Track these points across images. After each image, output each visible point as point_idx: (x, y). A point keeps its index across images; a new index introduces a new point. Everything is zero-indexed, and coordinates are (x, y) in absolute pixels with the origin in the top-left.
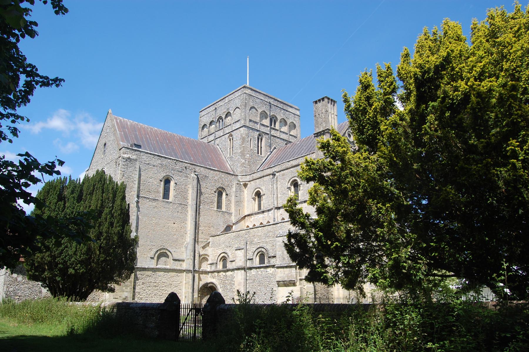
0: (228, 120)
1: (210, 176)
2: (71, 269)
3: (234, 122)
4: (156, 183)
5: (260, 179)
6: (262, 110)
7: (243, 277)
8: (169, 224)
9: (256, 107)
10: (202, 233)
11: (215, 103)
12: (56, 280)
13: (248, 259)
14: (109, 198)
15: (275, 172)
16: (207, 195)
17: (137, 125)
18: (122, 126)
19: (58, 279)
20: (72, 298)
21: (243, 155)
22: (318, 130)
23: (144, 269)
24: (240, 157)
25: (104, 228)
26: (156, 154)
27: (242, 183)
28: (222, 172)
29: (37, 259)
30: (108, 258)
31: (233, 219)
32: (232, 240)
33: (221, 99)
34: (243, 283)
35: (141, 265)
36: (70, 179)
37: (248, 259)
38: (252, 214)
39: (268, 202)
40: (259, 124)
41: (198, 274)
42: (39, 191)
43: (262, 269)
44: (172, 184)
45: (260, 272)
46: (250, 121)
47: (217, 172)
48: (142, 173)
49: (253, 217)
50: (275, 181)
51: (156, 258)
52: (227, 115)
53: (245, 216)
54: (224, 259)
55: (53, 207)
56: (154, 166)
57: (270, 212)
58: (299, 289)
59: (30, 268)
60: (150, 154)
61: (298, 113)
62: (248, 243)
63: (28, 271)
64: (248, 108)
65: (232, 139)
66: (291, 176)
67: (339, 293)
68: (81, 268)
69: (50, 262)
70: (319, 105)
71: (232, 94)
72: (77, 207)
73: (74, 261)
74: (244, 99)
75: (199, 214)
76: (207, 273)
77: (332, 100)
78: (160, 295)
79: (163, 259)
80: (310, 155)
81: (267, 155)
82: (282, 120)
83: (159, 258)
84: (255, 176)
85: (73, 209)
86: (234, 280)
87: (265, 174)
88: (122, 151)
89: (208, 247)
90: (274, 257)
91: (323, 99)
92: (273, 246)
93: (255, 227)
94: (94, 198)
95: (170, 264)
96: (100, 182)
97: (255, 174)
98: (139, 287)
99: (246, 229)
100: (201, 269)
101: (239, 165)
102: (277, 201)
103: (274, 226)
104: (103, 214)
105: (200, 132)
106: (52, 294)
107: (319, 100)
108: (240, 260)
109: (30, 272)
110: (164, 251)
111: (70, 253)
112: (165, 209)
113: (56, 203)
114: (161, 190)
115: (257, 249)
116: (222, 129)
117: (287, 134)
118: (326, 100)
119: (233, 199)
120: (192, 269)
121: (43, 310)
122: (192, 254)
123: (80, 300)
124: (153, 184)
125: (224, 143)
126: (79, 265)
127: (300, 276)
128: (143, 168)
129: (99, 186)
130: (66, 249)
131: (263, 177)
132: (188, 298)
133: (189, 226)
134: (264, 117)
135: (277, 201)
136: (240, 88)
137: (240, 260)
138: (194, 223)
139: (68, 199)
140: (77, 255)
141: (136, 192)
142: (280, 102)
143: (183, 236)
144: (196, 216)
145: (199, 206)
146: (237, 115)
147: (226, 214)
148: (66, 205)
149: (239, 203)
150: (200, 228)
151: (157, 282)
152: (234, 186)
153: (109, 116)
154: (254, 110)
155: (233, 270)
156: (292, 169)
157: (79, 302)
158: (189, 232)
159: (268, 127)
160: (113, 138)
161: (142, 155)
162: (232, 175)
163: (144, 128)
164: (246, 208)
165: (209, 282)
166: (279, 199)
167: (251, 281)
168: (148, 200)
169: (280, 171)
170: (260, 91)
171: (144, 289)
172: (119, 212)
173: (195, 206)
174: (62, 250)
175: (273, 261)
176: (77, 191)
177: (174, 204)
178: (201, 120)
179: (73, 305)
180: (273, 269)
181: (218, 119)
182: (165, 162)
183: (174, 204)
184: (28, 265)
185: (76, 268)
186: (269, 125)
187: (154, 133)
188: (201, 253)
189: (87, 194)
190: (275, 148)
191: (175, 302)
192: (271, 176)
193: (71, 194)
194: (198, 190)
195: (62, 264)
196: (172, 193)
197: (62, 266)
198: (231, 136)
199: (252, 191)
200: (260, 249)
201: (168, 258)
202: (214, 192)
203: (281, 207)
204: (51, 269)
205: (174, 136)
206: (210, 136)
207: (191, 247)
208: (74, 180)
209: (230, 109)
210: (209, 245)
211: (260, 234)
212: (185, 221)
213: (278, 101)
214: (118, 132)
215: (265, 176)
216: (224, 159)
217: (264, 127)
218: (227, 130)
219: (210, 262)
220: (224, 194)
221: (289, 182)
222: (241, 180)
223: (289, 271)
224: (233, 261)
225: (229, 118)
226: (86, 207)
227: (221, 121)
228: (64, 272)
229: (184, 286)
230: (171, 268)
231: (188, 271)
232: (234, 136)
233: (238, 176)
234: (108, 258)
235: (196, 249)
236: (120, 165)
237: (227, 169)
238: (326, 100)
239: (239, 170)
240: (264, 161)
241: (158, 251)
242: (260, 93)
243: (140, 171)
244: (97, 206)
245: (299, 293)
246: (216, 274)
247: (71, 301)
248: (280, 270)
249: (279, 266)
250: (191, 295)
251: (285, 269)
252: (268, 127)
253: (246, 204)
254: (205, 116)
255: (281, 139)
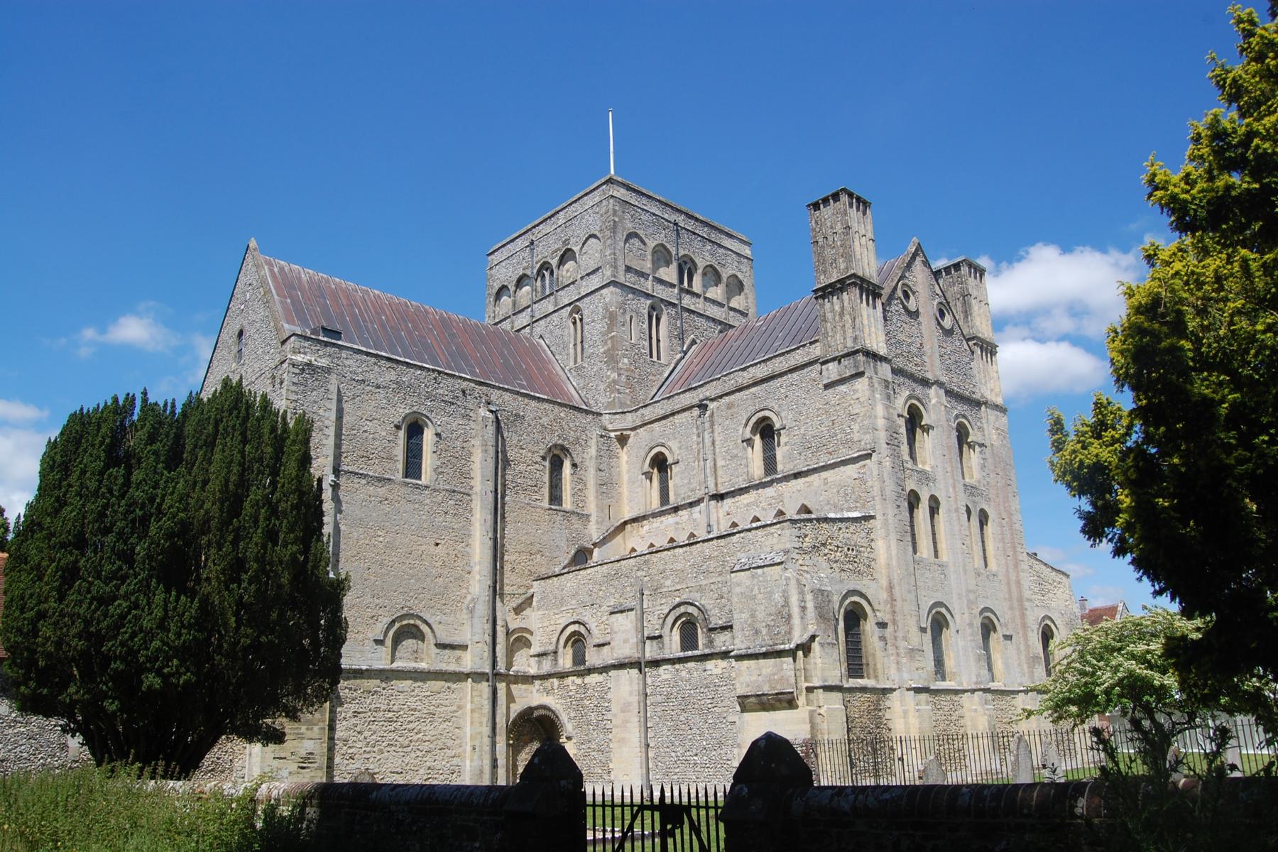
0: (568, 271)
1: (530, 416)
2: (151, 676)
3: (584, 274)
4: (384, 434)
5: (664, 422)
6: (656, 243)
7: (636, 687)
8: (423, 548)
9: (641, 233)
10: (513, 570)
11: (530, 230)
12: (103, 709)
13: (649, 638)
14: (262, 458)
15: (707, 399)
16: (522, 467)
17: (327, 282)
18: (287, 285)
19: (111, 706)
20: (155, 769)
21: (611, 358)
22: (823, 281)
23: (358, 674)
24: (604, 367)
25: (251, 548)
26: (384, 354)
27: (612, 435)
28: (560, 404)
29: (44, 645)
30: (263, 639)
31: (594, 532)
32: (598, 587)
33: (546, 216)
34: (636, 705)
35: (350, 662)
36: (145, 400)
37: (649, 638)
38: (644, 517)
39: (689, 483)
40: (651, 278)
41: (504, 684)
42: (50, 439)
43: (691, 665)
44: (428, 436)
45: (684, 674)
46: (628, 269)
47: (546, 406)
48: (345, 406)
49: (647, 526)
50: (707, 425)
51: (389, 642)
52: (562, 256)
53: (625, 523)
54: (577, 641)
55: (93, 485)
56: (378, 387)
57: (697, 509)
58: (806, 715)
59: (24, 675)
60: (368, 354)
61: (747, 251)
62: (646, 592)
63: (17, 684)
64: (621, 236)
65: (581, 320)
66: (752, 409)
67: (906, 723)
68: (183, 670)
69: (83, 654)
70: (826, 212)
71: (575, 201)
72: (166, 482)
73: (158, 650)
74: (611, 212)
75: (503, 517)
76: (528, 679)
77: (859, 200)
78: (402, 746)
79: (409, 644)
80: (806, 349)
81: (674, 361)
82: (709, 269)
83: (397, 641)
84: (649, 413)
85: (154, 488)
86: (609, 696)
87: (677, 407)
88: (288, 346)
89: (529, 609)
90: (727, 628)
91: (836, 197)
92: (722, 597)
93: (673, 545)
94: (217, 456)
95: (430, 659)
96: (235, 412)
97: (649, 408)
98: (344, 723)
99: (668, 546)
100: (513, 669)
101: (602, 387)
102: (716, 479)
103: (722, 542)
104: (247, 505)
105: (491, 307)
106: (93, 754)
107: (825, 201)
108: (626, 641)
109: (23, 688)
110: (412, 622)
111: (146, 623)
112: (410, 507)
113: (102, 473)
114: (399, 452)
115: (674, 608)
116: (552, 294)
117: (721, 305)
118: (844, 198)
119: (591, 476)
120: (487, 670)
121: (60, 809)
122: (488, 627)
123: (180, 773)
124: (377, 436)
125: (557, 332)
126: (175, 662)
127: (806, 680)
128: (348, 394)
129: (231, 424)
130: (134, 612)
131: (673, 414)
132: (481, 751)
133: (478, 551)
134: (662, 263)
135: (716, 479)
136: (596, 185)
137: (626, 641)
138: (490, 543)
139: (139, 462)
140: (169, 631)
141: (331, 458)
142: (702, 222)
143: (461, 578)
144: (496, 522)
145: (503, 497)
146: (591, 255)
147: (574, 519)
148: (133, 478)
149: (607, 486)
150: (506, 558)
151: (395, 708)
152: (593, 443)
153: (249, 258)
154: (635, 241)
155: (604, 669)
156: (753, 390)
157: (179, 779)
158: (477, 568)
159: (672, 286)
160: (262, 312)
161: (344, 355)
162: (587, 412)
163: (346, 291)
164: (626, 501)
165: (534, 703)
166: (720, 472)
167: (659, 698)
168: (364, 482)
169: (721, 397)
170: (651, 194)
171: (358, 729)
172: (294, 499)
173: (491, 497)
174: (122, 617)
175: (722, 641)
176: (167, 435)
177: (435, 490)
178: (492, 276)
179: (159, 790)
180: (722, 664)
181: (539, 271)
182: (408, 376)
183: (435, 490)
184: (16, 666)
185: (166, 670)
186: (675, 281)
187: (372, 302)
188: (512, 627)
189: (196, 446)
190: (694, 342)
191: (563, 783)
192: (696, 412)
193: (146, 445)
194: (497, 452)
195: (122, 658)
196: (428, 461)
197: (122, 667)
198: (578, 310)
199: (643, 454)
200: (682, 609)
201: (423, 640)
202: (539, 459)
203: (727, 493)
204: (88, 676)
205: (426, 312)
206: (520, 316)
207: (483, 609)
208: (156, 404)
209: (572, 240)
210: (531, 603)
211: (679, 566)
212: (464, 537)
213: (697, 219)
214: (276, 297)
215: (678, 412)
216: (561, 373)
217: (663, 287)
218: (566, 297)
219: (535, 649)
220: (567, 465)
221: (746, 425)
222: (610, 427)
223: (775, 665)
224: (603, 645)
225: (570, 265)
226: (195, 483)
227: (547, 274)
228: (127, 684)
229: (468, 719)
230: (432, 669)
231: (477, 676)
232: (585, 312)
233: (601, 414)
234: (263, 639)
235: (499, 614)
236: (285, 383)
237: (570, 398)
238: (844, 198)
239: (603, 400)
240: (666, 375)
241: (393, 622)
242: (649, 197)
243: (339, 401)
244: (227, 481)
245: (808, 727)
246: (555, 681)
247: (152, 778)
248: (746, 663)
249: (743, 652)
250: (487, 741)
251: (762, 661)
252: (672, 286)
253: (625, 490)
254: (503, 264)
255: (708, 318)
